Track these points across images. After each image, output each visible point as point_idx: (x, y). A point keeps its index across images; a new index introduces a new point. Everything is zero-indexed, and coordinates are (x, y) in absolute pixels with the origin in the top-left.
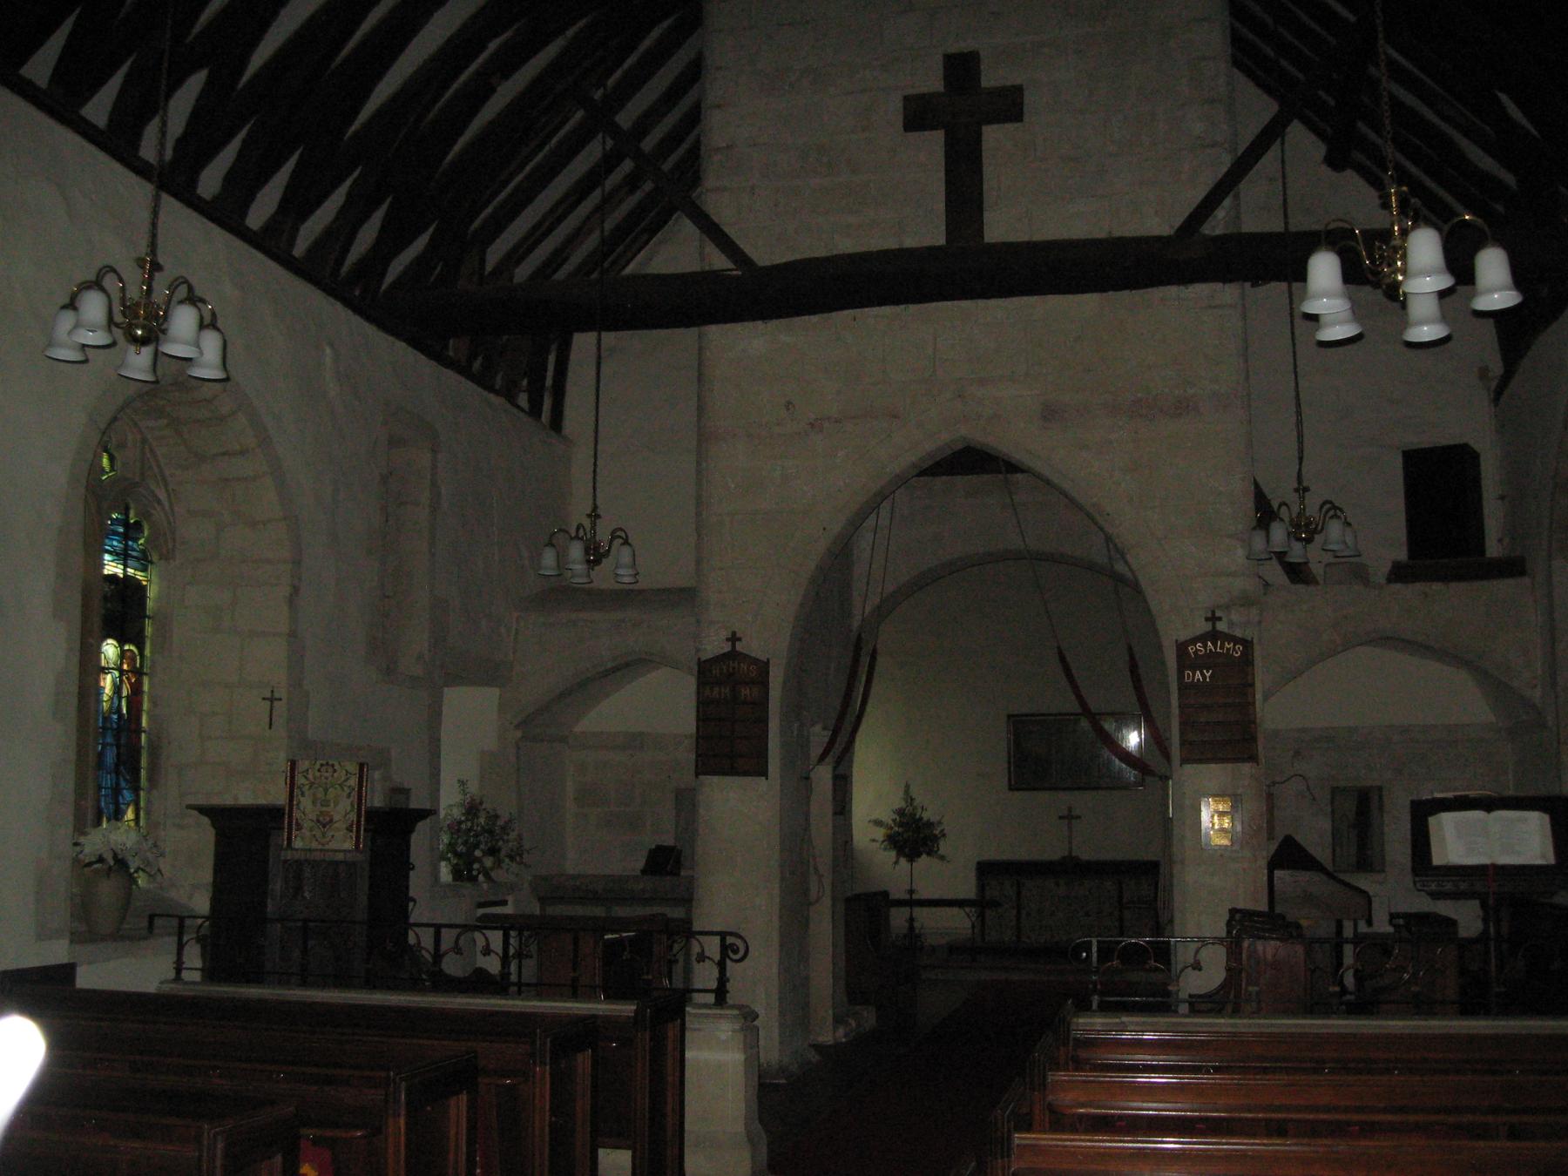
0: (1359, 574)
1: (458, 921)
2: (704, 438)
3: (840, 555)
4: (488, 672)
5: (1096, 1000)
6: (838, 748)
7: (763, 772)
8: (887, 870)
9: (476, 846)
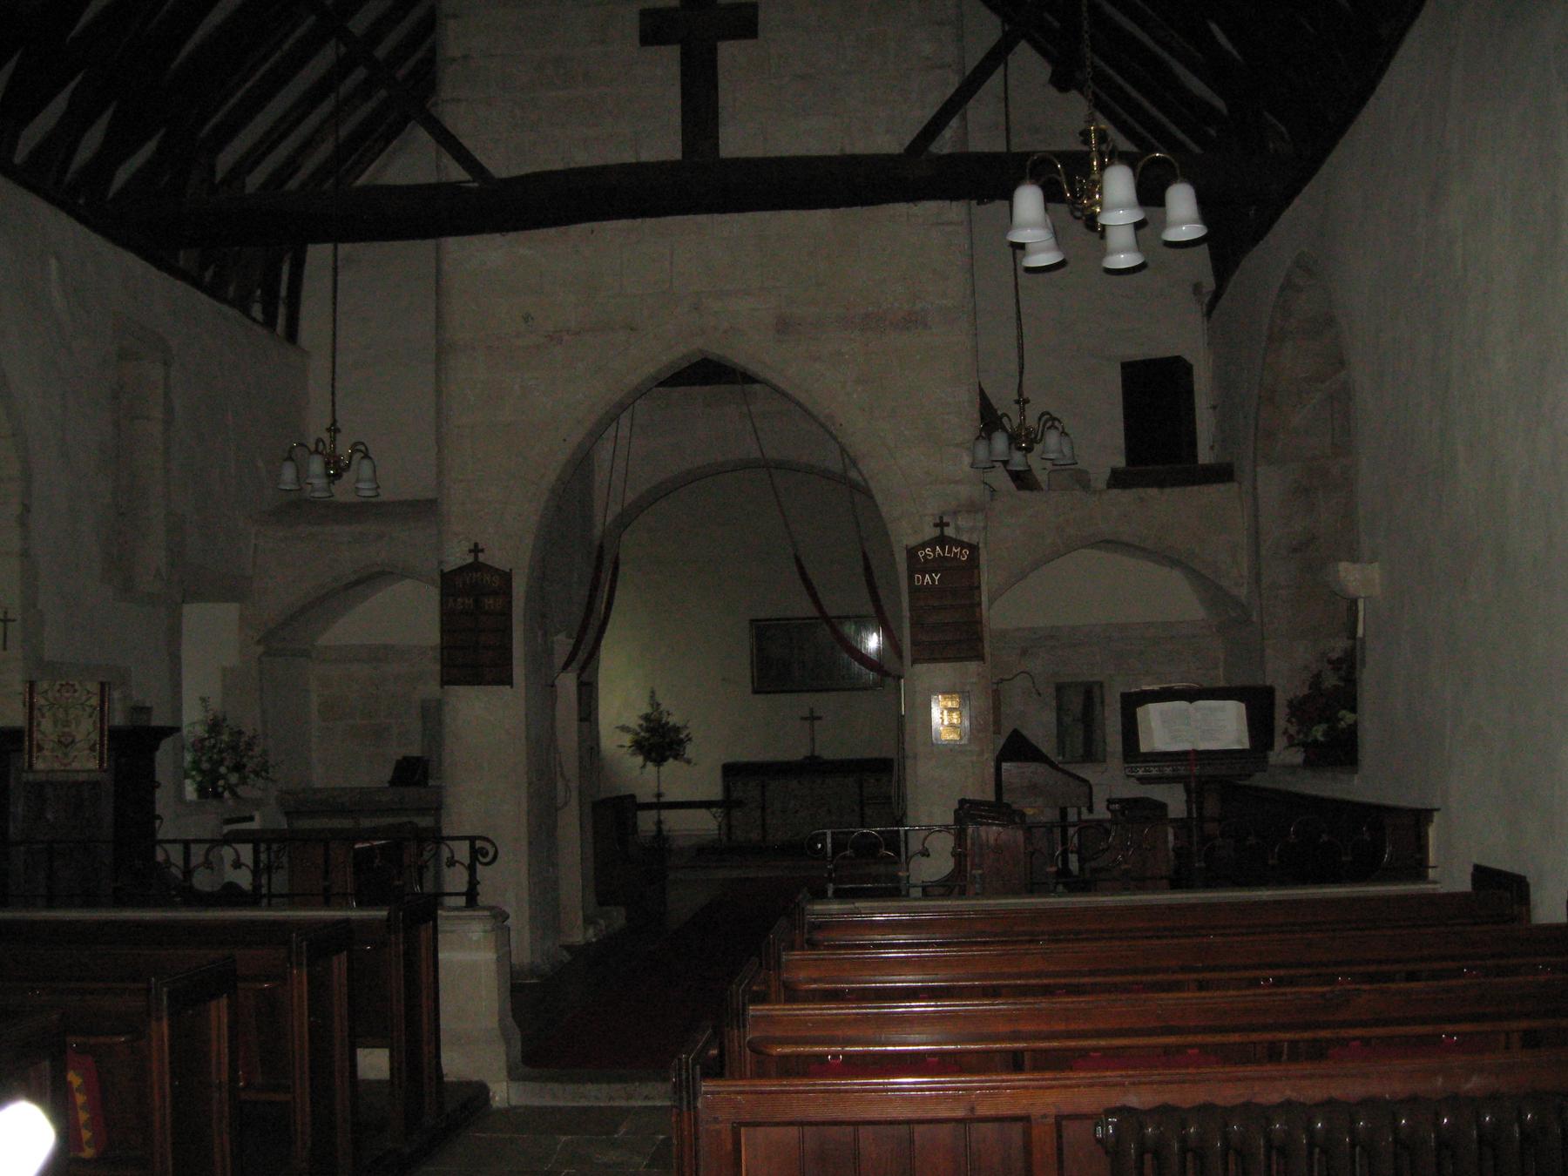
0: (1081, 480)
1: (208, 836)
2: (443, 351)
3: (581, 465)
4: (232, 589)
5: (831, 888)
6: (582, 655)
7: (508, 681)
8: (637, 776)
9: (221, 762)
